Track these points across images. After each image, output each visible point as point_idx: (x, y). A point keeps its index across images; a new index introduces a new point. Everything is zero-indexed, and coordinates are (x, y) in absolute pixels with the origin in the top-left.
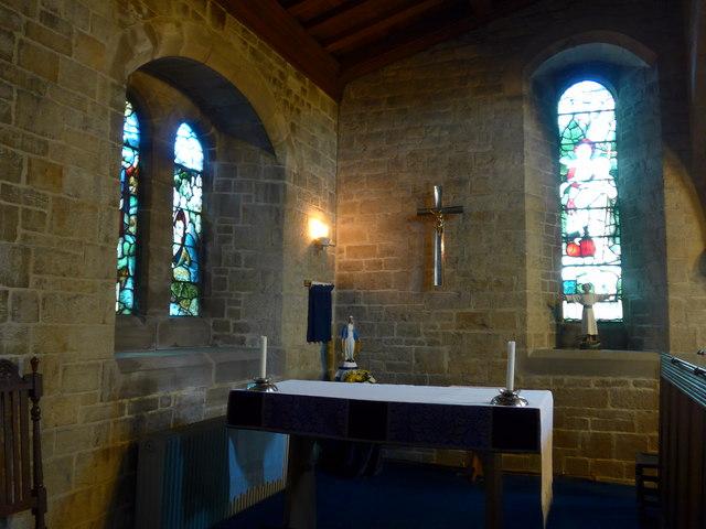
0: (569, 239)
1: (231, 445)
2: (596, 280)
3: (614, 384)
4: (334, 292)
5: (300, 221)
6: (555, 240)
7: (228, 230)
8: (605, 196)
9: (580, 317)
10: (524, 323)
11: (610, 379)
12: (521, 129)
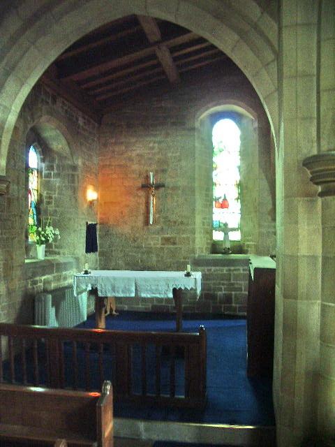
0: (217, 200)
1: (252, 275)
2: (229, 219)
3: (235, 270)
4: (98, 227)
5: (84, 192)
6: (209, 201)
7: (50, 198)
8: (223, 148)
9: (222, 239)
10: (194, 241)
11: (232, 268)
12: (194, 146)
